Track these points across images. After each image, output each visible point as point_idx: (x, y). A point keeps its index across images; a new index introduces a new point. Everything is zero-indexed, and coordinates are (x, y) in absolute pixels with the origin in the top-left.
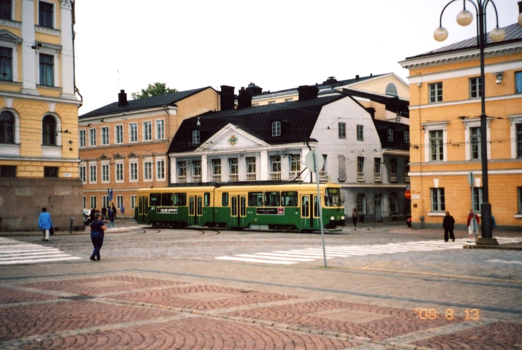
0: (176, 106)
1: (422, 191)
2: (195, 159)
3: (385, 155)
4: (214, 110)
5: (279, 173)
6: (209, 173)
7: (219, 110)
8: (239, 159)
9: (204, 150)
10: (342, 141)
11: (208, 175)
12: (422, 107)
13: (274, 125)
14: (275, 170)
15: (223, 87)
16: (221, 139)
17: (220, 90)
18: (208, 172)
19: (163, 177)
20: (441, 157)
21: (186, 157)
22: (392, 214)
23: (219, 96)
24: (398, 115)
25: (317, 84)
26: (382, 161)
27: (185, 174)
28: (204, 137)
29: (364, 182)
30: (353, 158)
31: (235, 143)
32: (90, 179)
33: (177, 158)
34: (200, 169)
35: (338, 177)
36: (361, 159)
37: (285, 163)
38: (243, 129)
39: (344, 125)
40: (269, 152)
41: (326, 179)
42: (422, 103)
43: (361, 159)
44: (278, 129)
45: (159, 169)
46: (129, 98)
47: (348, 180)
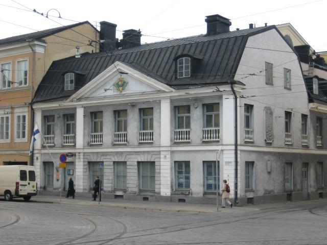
0: (44, 42)
2: (66, 112)
3: (311, 111)
4: (91, 52)
5: (217, 128)
6: (86, 131)
7: (98, 51)
8: (128, 111)
9: (79, 100)
10: (269, 88)
11: (84, 133)
13: (181, 63)
14: (180, 126)
15: (104, 24)
16: (105, 82)
19: (24, 136)
21: (55, 110)
22: (319, 189)
23: (98, 35)
24: (310, 66)
25: (217, 23)
26: (309, 117)
27: (53, 133)
28: (81, 81)
30: (279, 113)
31: (123, 89)
32: (15, 134)
34: (74, 125)
35: (265, 138)
36: (288, 115)
37: (197, 116)
38: (162, 42)
40: (172, 101)
43: (288, 115)
44: (187, 67)
45: (19, 125)
47: (275, 143)
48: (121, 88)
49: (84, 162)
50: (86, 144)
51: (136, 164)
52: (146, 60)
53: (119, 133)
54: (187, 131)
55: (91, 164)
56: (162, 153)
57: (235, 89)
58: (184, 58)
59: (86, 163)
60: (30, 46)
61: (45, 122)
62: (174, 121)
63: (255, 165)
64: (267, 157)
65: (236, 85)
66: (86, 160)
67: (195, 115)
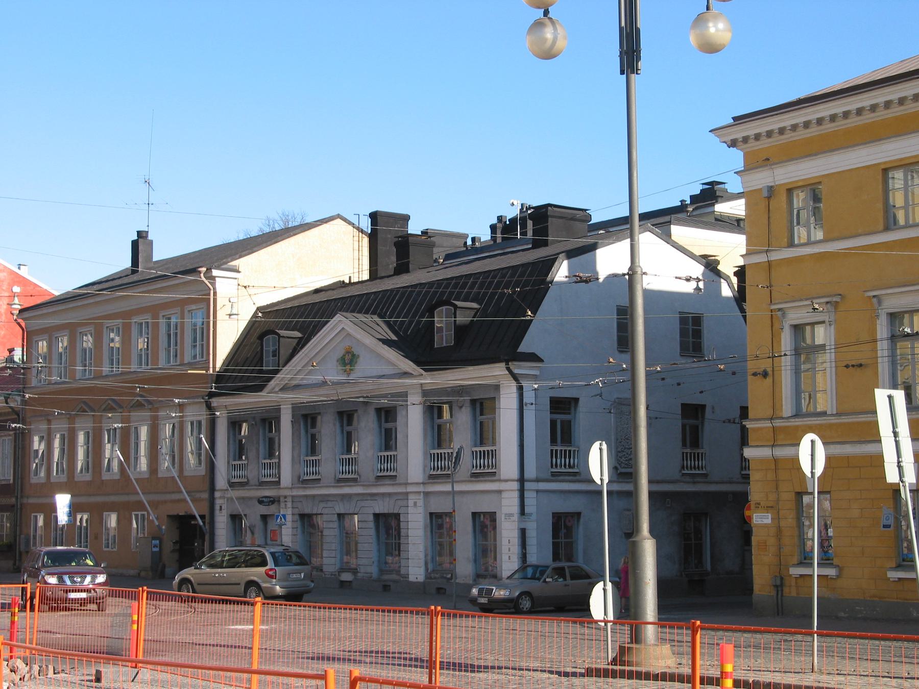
1: (778, 500)
18: (293, 448)
29: (705, 475)
41: (392, 474)
46: (161, 253)
48: (348, 367)
51: (371, 518)
53: (482, 449)
56: (411, 497)
58: (444, 308)
59: (297, 517)
63: (582, 520)
66: (296, 511)
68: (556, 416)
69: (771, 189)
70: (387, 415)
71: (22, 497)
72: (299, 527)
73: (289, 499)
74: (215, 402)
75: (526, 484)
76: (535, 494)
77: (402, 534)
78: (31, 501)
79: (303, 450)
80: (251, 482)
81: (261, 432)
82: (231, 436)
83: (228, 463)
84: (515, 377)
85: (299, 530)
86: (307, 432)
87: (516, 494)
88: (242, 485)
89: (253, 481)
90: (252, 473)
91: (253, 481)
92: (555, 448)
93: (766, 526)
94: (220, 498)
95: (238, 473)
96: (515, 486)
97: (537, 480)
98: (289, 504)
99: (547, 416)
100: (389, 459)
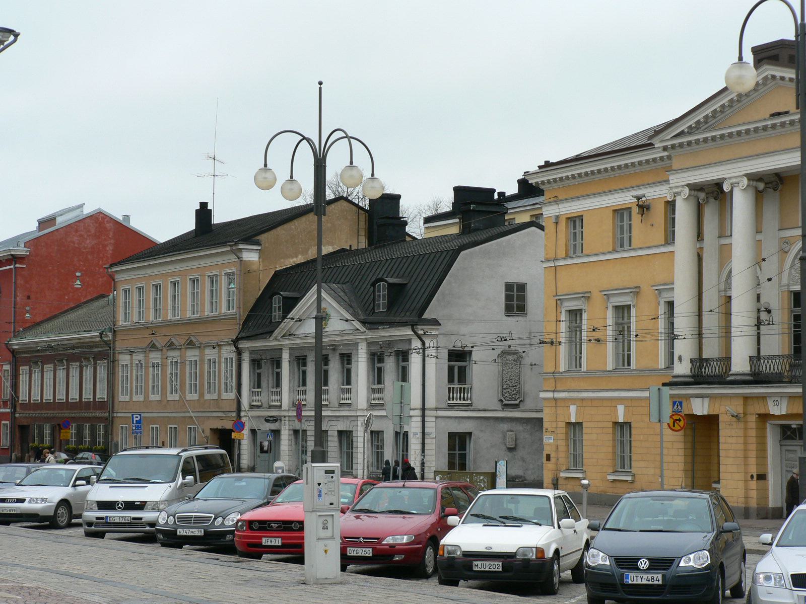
12: (558, 263)
17: (365, 204)
20: (629, 364)
33: (252, 352)
39: (522, 287)
42: (559, 256)
49: (289, 430)
50: (291, 405)
51: (336, 433)
52: (394, 273)
54: (461, 388)
55: (296, 432)
56: (360, 419)
57: (240, 346)
58: (381, 283)
59: (292, 432)
60: (233, 252)
61: (254, 369)
62: (371, 373)
63: (473, 438)
64: (505, 426)
65: (419, 327)
66: (291, 428)
67: (388, 367)
68: (452, 363)
69: (557, 217)
70: (347, 359)
71: (113, 412)
72: (293, 440)
73: (287, 419)
74: (243, 345)
75: (426, 412)
76: (434, 419)
77: (354, 446)
78: (119, 415)
79: (296, 383)
80: (264, 406)
81: (270, 369)
82: (252, 370)
83: (250, 390)
84: (419, 337)
85: (293, 443)
86: (299, 369)
87: (419, 419)
88: (258, 407)
89: (265, 405)
90: (264, 398)
91: (265, 405)
92: (452, 386)
93: (550, 445)
94: (245, 416)
95: (377, 395)
96: (419, 413)
97: (437, 409)
98: (287, 423)
99: (445, 364)
100: (380, 391)
